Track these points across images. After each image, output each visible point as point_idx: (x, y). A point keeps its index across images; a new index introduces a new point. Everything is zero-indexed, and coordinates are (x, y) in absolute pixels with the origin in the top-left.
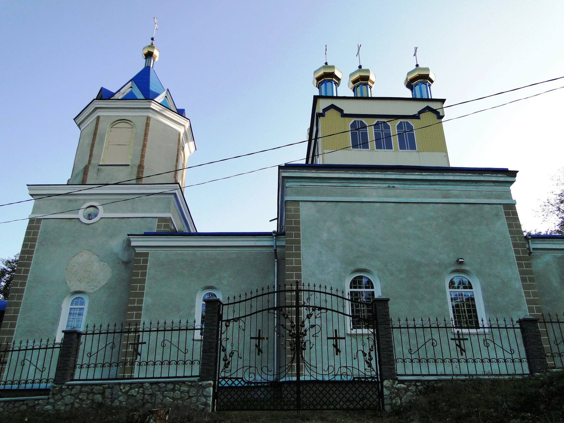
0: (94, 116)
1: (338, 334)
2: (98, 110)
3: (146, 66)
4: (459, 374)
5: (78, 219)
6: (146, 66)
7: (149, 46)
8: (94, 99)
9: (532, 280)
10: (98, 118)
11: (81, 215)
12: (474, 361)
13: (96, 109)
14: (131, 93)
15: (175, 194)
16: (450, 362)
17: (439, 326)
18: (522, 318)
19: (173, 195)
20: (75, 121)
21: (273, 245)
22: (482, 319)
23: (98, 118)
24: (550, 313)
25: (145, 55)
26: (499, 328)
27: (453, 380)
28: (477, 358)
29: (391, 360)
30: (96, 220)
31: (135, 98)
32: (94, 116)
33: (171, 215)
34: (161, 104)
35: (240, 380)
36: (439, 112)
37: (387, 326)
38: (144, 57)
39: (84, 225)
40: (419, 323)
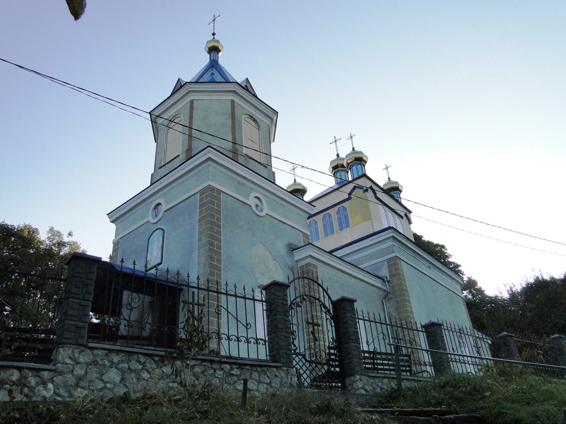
0: (187, 100)
1: (196, 298)
2: (191, 94)
4: (265, 360)
9: (211, 229)
10: (192, 102)
12: (238, 340)
16: (217, 337)
17: (228, 293)
18: (335, 299)
22: (227, 283)
23: (192, 102)
24: (136, 261)
25: (209, 48)
26: (254, 300)
28: (241, 336)
29: (84, 314)
32: (187, 100)
35: (301, 357)
36: (218, 47)
37: (284, 301)
38: (207, 49)
40: (240, 291)
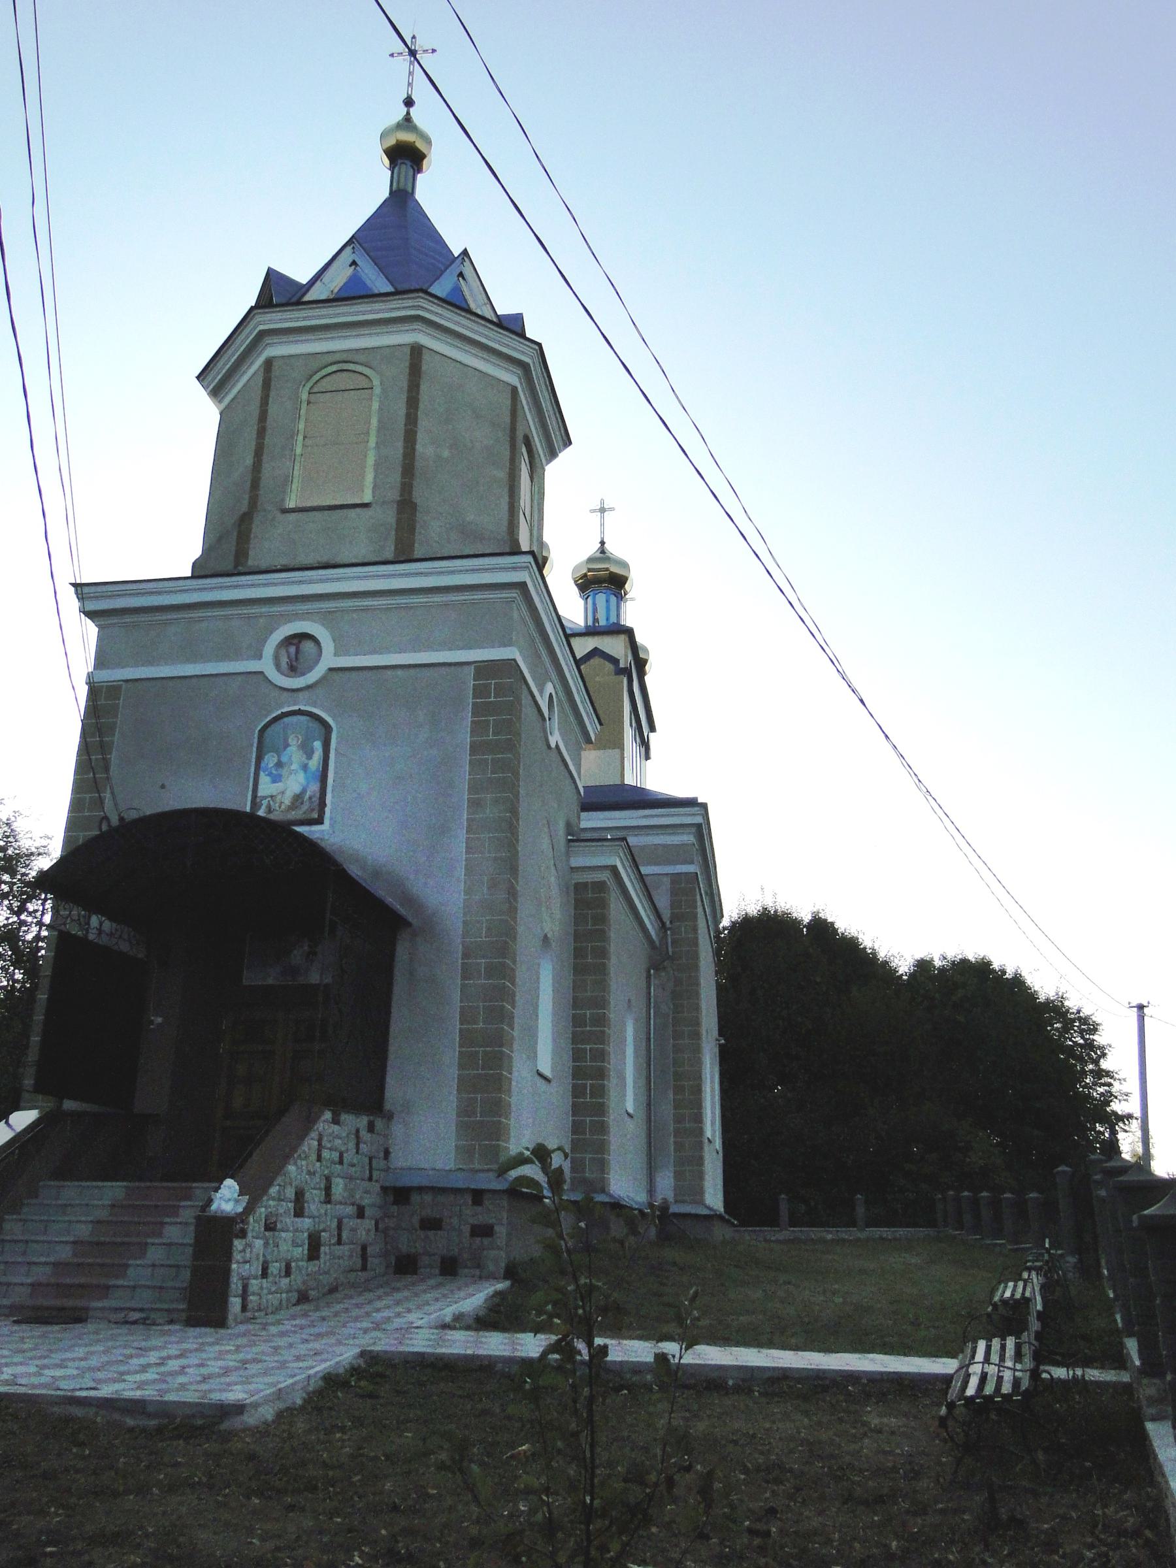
2: (268, 340)
3: (394, 189)
5: (262, 673)
6: (394, 189)
7: (399, 126)
8: (252, 309)
11: (266, 666)
13: (262, 334)
14: (354, 280)
15: (522, 586)
19: (518, 591)
20: (446, 268)
21: (582, 813)
23: (269, 364)
27: (680, 1340)
30: (294, 687)
31: (362, 293)
33: (518, 653)
34: (449, 299)
39: (285, 694)
